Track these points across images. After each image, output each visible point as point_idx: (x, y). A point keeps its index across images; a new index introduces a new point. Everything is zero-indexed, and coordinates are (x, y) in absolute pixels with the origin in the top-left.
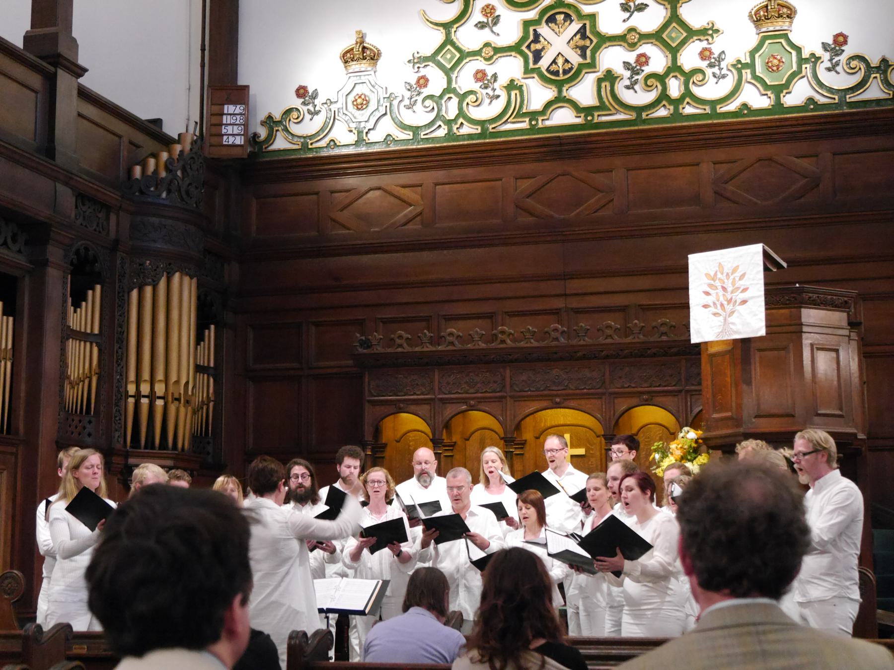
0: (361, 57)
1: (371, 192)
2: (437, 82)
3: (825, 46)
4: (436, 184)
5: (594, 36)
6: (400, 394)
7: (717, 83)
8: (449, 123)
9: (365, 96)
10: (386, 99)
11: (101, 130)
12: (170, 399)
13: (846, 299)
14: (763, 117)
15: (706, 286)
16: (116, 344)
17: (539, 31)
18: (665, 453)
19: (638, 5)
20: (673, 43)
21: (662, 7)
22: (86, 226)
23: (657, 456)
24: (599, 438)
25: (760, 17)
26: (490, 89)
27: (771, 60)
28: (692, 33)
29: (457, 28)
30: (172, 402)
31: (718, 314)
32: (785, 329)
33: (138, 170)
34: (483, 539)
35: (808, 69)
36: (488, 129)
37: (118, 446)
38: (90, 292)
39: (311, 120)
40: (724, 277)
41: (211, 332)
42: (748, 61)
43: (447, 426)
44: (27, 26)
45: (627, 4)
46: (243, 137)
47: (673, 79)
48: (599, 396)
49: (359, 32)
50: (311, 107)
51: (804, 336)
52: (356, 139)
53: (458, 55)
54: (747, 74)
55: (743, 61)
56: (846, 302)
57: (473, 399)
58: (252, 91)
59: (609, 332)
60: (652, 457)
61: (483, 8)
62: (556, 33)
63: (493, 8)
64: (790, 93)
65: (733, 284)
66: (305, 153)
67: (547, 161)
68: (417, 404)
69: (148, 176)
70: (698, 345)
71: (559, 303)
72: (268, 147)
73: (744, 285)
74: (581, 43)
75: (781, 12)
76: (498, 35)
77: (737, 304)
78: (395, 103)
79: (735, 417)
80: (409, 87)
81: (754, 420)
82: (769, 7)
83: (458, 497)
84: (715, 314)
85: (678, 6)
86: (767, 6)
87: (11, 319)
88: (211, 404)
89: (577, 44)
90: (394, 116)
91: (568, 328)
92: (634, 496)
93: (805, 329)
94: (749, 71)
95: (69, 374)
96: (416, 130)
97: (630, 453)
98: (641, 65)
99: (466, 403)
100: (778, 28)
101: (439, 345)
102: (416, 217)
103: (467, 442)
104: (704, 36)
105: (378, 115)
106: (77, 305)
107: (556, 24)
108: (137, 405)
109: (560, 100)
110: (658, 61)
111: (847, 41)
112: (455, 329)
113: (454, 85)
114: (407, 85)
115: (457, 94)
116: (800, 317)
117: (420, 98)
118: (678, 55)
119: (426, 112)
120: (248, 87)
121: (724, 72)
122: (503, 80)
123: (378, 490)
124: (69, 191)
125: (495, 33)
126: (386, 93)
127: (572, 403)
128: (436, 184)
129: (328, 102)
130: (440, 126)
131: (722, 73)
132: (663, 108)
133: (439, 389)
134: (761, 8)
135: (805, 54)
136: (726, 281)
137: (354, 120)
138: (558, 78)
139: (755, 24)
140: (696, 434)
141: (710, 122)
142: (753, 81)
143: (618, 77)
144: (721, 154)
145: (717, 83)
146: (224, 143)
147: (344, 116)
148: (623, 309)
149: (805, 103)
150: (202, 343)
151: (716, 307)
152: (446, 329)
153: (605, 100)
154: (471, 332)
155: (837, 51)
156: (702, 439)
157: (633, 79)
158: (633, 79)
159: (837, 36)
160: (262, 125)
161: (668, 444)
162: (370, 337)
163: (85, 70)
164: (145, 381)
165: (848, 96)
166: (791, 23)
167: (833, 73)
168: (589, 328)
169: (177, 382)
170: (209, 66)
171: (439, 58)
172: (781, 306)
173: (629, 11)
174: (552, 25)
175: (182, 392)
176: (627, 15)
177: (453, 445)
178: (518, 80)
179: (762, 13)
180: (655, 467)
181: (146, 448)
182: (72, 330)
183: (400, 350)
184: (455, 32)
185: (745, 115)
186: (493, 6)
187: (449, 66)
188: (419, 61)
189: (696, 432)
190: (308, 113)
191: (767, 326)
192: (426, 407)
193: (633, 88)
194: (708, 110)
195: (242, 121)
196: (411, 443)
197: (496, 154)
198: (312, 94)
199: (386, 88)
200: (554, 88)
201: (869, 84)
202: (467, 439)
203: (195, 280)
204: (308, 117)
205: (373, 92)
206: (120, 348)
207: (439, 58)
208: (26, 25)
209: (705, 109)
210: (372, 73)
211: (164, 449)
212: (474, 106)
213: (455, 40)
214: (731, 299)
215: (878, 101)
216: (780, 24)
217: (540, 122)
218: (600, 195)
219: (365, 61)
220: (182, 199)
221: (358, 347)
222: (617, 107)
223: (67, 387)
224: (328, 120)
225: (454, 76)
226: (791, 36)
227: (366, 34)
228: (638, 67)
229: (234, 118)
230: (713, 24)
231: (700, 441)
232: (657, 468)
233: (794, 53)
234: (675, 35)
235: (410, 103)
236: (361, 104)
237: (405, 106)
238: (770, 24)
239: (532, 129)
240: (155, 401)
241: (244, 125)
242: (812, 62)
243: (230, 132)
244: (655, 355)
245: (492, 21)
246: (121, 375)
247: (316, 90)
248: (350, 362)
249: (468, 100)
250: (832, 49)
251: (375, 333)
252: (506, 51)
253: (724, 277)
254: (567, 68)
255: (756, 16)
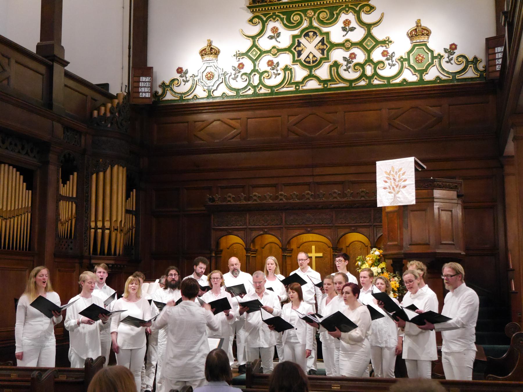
0: (210, 53)
1: (215, 122)
2: (248, 66)
3: (445, 50)
4: (248, 118)
5: (328, 44)
6: (229, 225)
7: (390, 68)
8: (254, 87)
9: (212, 73)
10: (222, 75)
11: (77, 93)
12: (112, 229)
13: (456, 184)
14: (414, 86)
15: (385, 178)
16: (84, 203)
17: (301, 40)
18: (363, 261)
19: (351, 28)
20: (368, 47)
21: (363, 29)
22: (69, 143)
23: (360, 263)
24: (329, 248)
25: (413, 35)
26: (275, 70)
27: (418, 57)
28: (378, 43)
29: (259, 38)
30: (114, 231)
31: (391, 192)
32: (426, 200)
33: (95, 113)
34: (270, 308)
35: (437, 62)
36: (274, 90)
37: (86, 254)
38: (71, 176)
39: (184, 85)
40: (394, 173)
41: (134, 193)
42: (406, 57)
43: (253, 241)
44: (38, 40)
45: (345, 27)
46: (150, 93)
47: (368, 66)
48: (330, 228)
49: (209, 40)
50: (184, 78)
51: (435, 204)
52: (207, 95)
53: (259, 53)
54: (406, 64)
55: (404, 58)
56: (456, 186)
57: (266, 228)
58: (154, 70)
59: (335, 195)
60: (356, 264)
61: (272, 29)
62: (309, 42)
63: (277, 29)
64: (427, 74)
65: (399, 177)
66: (181, 102)
67: (304, 107)
68: (238, 231)
69: (101, 116)
70: (381, 208)
71: (310, 180)
72: (163, 98)
73: (405, 178)
74: (322, 47)
75: (423, 32)
76: (280, 42)
77: (401, 187)
78: (227, 76)
79: (399, 244)
80: (234, 69)
81: (409, 246)
82: (417, 30)
83: (259, 287)
84: (390, 192)
85: (371, 28)
86: (416, 29)
87: (30, 191)
88: (134, 230)
89: (320, 48)
90: (226, 83)
91: (314, 194)
92: (349, 297)
93: (435, 200)
94: (406, 62)
95: (61, 218)
96: (237, 90)
97: (345, 261)
98: (352, 59)
99: (262, 230)
100: (422, 41)
101: (249, 201)
102: (237, 135)
103: (263, 249)
104: (384, 44)
105: (218, 83)
106: (64, 183)
107: (309, 37)
108: (96, 233)
109: (311, 76)
110: (361, 57)
111: (456, 48)
112: (257, 193)
113: (257, 68)
114: (233, 68)
115: (259, 73)
116: (433, 194)
117: (240, 75)
118: (371, 54)
119: (243, 81)
120: (152, 68)
121: (394, 63)
122: (282, 66)
123: (217, 282)
124: (60, 125)
125: (278, 41)
126: (223, 72)
127: (316, 231)
128: (248, 118)
129: (193, 76)
130: (250, 89)
131: (393, 63)
132: (363, 81)
133: (249, 223)
134: (414, 30)
135: (435, 54)
136: (395, 175)
137: (206, 85)
138: (310, 65)
139: (410, 38)
140: (379, 252)
141: (387, 88)
142: (409, 68)
143: (340, 65)
144: (392, 104)
145: (390, 68)
146: (140, 96)
147: (201, 83)
148: (342, 183)
149: (435, 79)
150: (129, 199)
151: (390, 189)
152: (253, 193)
153: (334, 76)
154: (265, 195)
155: (452, 52)
156: (382, 255)
157: (348, 66)
158: (348, 66)
159: (451, 45)
160: (160, 87)
161: (365, 257)
162: (214, 196)
163: (68, 63)
164: (100, 221)
165: (457, 76)
166: (428, 38)
167: (449, 64)
168: (325, 193)
169: (116, 221)
170: (133, 57)
171: (249, 54)
172: (423, 188)
173: (346, 31)
174: (307, 38)
175: (119, 226)
176: (345, 33)
177: (256, 251)
178: (290, 65)
179: (414, 33)
180: (358, 268)
181: (100, 254)
182: (62, 196)
183: (229, 203)
184: (258, 40)
185: (404, 85)
186: (277, 28)
187: (254, 58)
188: (239, 55)
189: (379, 251)
190: (183, 81)
191: (416, 199)
192: (242, 232)
193: (348, 70)
194: (386, 82)
195: (149, 85)
196: (235, 250)
197: (278, 103)
198: (185, 71)
199: (223, 69)
200: (308, 70)
201: (467, 70)
202: (263, 248)
203: (125, 168)
204: (183, 83)
205: (216, 71)
206: (87, 204)
207: (249, 54)
208: (37, 39)
209: (384, 82)
210: (215, 61)
211: (110, 255)
212: (267, 79)
213: (257, 45)
214: (398, 185)
215: (472, 79)
216: (423, 39)
217: (301, 87)
218: (331, 125)
219: (212, 55)
220: (119, 128)
221: (208, 202)
222: (339, 80)
223: (60, 225)
224: (193, 85)
225: (257, 63)
226: (428, 45)
227: (212, 41)
228: (351, 60)
229: (145, 84)
230: (388, 38)
231: (381, 255)
232: (359, 269)
233: (430, 54)
234: (369, 43)
235: (235, 77)
236: (210, 77)
237: (232, 78)
238: (417, 39)
239: (297, 91)
240: (105, 231)
241: (150, 87)
242: (439, 58)
243: (143, 91)
244: (358, 207)
245: (277, 35)
246: (87, 218)
247: (187, 69)
248: (204, 208)
249: (264, 76)
250: (449, 52)
251: (217, 195)
252: (283, 51)
253: (394, 173)
254: (314, 60)
255: (410, 34)
